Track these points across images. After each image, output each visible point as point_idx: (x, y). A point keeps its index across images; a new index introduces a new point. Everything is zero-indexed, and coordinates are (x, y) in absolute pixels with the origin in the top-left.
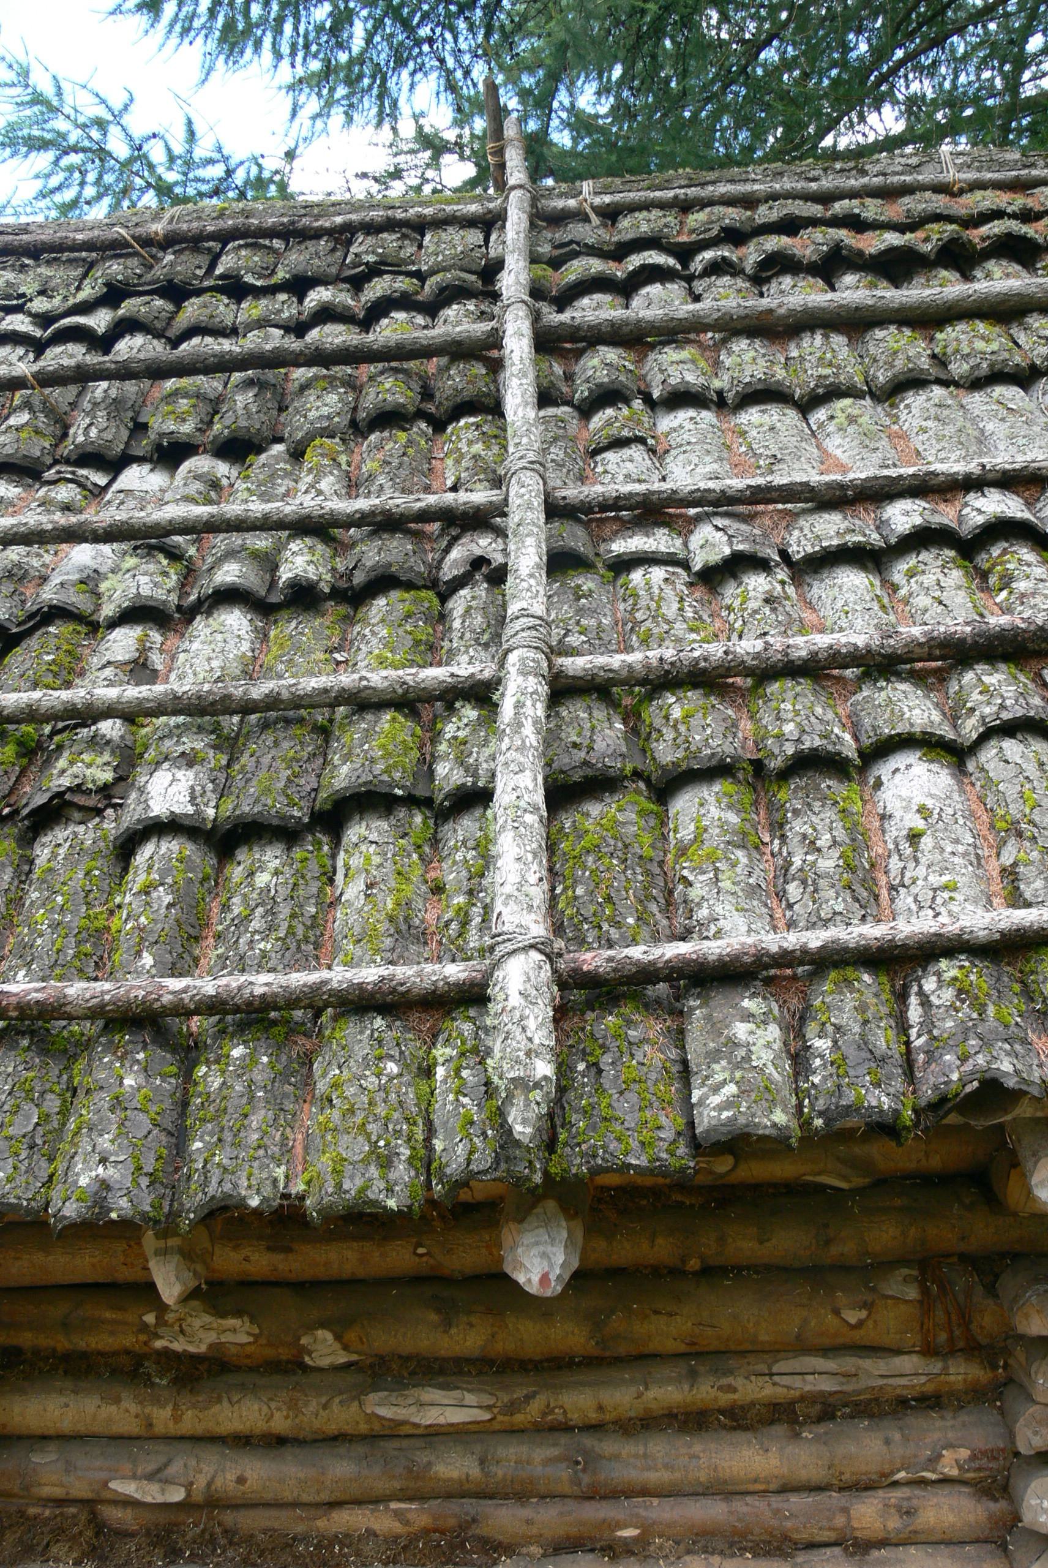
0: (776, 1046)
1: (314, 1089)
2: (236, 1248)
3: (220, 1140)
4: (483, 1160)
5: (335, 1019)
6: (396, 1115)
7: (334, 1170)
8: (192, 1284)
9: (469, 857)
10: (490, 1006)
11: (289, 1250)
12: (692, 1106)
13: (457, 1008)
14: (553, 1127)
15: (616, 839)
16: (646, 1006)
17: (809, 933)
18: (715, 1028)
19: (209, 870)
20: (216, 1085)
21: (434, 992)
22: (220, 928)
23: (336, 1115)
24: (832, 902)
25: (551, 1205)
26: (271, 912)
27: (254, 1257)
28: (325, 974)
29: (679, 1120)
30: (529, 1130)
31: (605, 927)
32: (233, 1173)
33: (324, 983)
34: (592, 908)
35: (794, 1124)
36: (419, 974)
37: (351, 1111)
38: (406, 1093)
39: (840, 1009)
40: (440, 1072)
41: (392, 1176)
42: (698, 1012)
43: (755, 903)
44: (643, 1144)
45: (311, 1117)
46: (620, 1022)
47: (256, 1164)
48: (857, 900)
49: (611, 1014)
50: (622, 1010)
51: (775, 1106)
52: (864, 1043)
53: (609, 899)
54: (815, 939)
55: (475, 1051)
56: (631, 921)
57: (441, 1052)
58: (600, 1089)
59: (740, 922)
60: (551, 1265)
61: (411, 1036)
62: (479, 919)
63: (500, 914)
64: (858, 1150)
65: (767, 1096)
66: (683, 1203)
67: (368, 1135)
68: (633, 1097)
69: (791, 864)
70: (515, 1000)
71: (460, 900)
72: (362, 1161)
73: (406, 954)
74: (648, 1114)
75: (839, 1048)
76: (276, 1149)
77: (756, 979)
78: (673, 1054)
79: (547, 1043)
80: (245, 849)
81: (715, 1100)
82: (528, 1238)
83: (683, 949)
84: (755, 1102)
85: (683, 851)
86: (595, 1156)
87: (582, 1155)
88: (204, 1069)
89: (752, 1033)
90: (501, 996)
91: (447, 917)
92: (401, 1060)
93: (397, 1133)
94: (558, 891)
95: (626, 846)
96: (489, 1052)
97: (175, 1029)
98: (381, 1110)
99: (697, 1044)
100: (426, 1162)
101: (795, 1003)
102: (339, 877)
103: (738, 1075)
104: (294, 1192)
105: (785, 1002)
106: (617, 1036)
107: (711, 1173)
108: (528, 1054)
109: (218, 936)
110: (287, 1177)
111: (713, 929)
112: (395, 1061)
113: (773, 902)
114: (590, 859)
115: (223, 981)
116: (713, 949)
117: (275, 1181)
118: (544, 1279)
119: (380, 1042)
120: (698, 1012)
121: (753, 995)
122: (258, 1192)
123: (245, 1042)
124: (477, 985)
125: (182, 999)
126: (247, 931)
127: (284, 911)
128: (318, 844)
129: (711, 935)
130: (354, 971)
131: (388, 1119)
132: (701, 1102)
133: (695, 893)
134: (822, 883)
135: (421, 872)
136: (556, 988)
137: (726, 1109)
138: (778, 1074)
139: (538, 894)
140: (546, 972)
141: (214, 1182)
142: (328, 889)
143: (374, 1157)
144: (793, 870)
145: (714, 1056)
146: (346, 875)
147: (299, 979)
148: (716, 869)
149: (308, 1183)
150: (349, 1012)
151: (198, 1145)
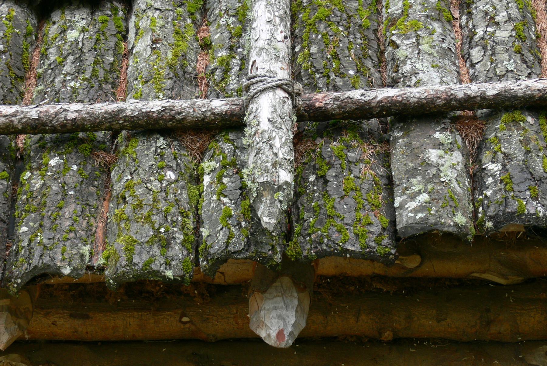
0: (459, 168)
1: (112, 190)
2: (46, 315)
3: (41, 226)
4: (238, 243)
5: (128, 139)
6: (173, 210)
7: (127, 249)
8: (18, 334)
9: (230, 22)
10: (246, 129)
11: (87, 317)
12: (394, 209)
13: (220, 132)
14: (290, 222)
15: (342, 11)
16: (362, 136)
17: (487, 84)
18: (413, 152)
19: (31, 27)
20: (38, 185)
21: (203, 120)
22: (40, 71)
23: (128, 209)
24: (505, 63)
25: (286, 280)
26: (79, 60)
27: (60, 322)
28: (121, 105)
29: (384, 219)
30: (273, 221)
31: (332, 76)
32: (51, 250)
33: (121, 111)
34: (323, 62)
35: (470, 225)
36: (192, 106)
37: (140, 206)
38: (181, 194)
39: (509, 142)
40: (207, 179)
41: (170, 254)
42: (400, 141)
43: (447, 62)
44: (357, 235)
45: (110, 210)
46: (342, 146)
47: (68, 243)
48: (525, 62)
49: (335, 140)
50: (344, 138)
51: (457, 210)
52: (526, 167)
53: (336, 56)
54: (492, 89)
55: (233, 164)
56: (351, 72)
57: (207, 164)
58: (326, 195)
59: (435, 75)
60: (285, 325)
61: (185, 153)
62: (237, 68)
63: (254, 62)
64: (515, 255)
65: (451, 203)
66: (381, 290)
67: (152, 224)
68: (350, 201)
69: (474, 34)
70: (265, 125)
71: (223, 53)
72: (147, 242)
73: (182, 93)
74: (361, 214)
75: (507, 170)
76: (83, 233)
77: (445, 118)
78: (381, 171)
79: (288, 157)
80: (59, 12)
81: (412, 205)
82: (268, 305)
83: (392, 92)
84: (442, 207)
85: (392, 22)
86: (321, 243)
87: (312, 242)
88: (28, 174)
89: (441, 157)
90: (255, 122)
91: (212, 66)
92: (177, 169)
93: (174, 223)
94: (297, 49)
95: (349, 17)
96: (244, 165)
97: (6, 144)
98: (162, 206)
99: (400, 162)
100: (195, 244)
101: (474, 136)
102: (131, 35)
103: (430, 187)
104: (96, 265)
105: (467, 136)
106: (339, 157)
107: (404, 268)
108: (274, 165)
109: (39, 77)
110: (91, 253)
111: (414, 80)
112: (173, 170)
113: (460, 62)
114: (322, 26)
115: (44, 108)
116: (414, 93)
117: (82, 256)
118: (280, 334)
119: (162, 156)
120: (400, 141)
121: (443, 130)
122: (70, 264)
123: (59, 155)
124: (236, 115)
125: (12, 121)
126: (61, 73)
127: (89, 59)
128: (115, 10)
129: (412, 84)
130: (143, 103)
131: (167, 212)
132: (401, 206)
133: (401, 53)
134: (499, 48)
135: (193, 33)
136: (295, 118)
137: (420, 211)
138: (460, 188)
139: (283, 48)
140: (288, 106)
141: (37, 255)
142: (123, 44)
143: (156, 240)
144: (476, 38)
145: (412, 173)
146: (136, 34)
147: (102, 108)
148: (418, 36)
149: (107, 258)
150: (138, 134)
151: (24, 229)
